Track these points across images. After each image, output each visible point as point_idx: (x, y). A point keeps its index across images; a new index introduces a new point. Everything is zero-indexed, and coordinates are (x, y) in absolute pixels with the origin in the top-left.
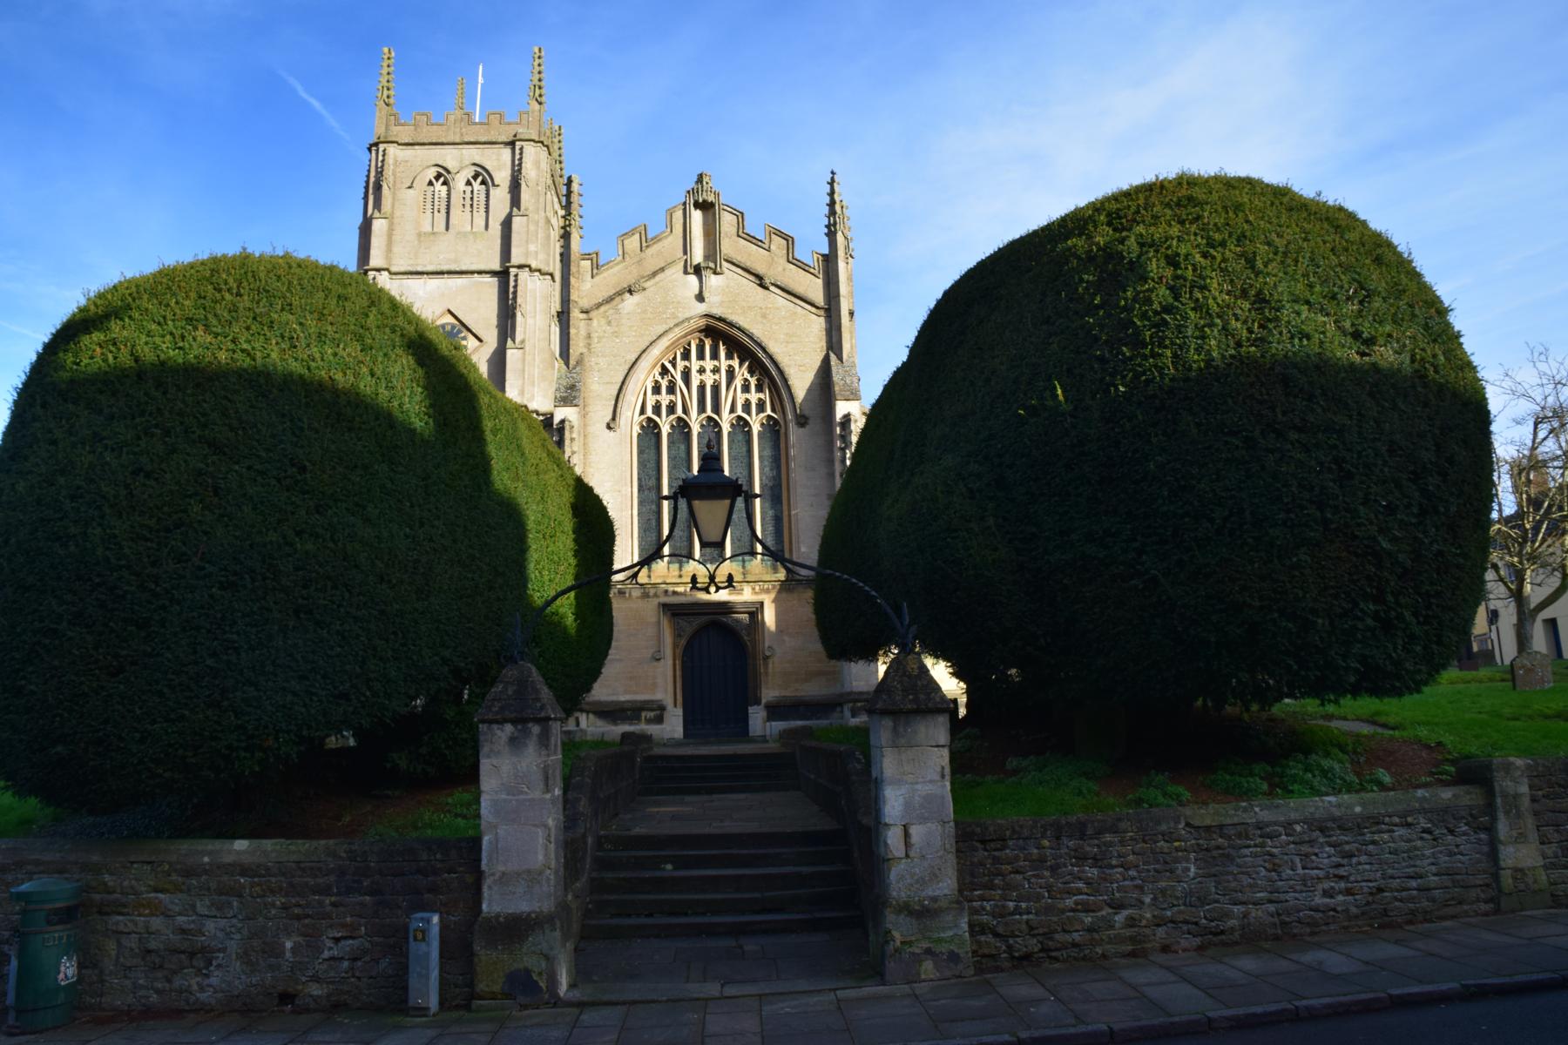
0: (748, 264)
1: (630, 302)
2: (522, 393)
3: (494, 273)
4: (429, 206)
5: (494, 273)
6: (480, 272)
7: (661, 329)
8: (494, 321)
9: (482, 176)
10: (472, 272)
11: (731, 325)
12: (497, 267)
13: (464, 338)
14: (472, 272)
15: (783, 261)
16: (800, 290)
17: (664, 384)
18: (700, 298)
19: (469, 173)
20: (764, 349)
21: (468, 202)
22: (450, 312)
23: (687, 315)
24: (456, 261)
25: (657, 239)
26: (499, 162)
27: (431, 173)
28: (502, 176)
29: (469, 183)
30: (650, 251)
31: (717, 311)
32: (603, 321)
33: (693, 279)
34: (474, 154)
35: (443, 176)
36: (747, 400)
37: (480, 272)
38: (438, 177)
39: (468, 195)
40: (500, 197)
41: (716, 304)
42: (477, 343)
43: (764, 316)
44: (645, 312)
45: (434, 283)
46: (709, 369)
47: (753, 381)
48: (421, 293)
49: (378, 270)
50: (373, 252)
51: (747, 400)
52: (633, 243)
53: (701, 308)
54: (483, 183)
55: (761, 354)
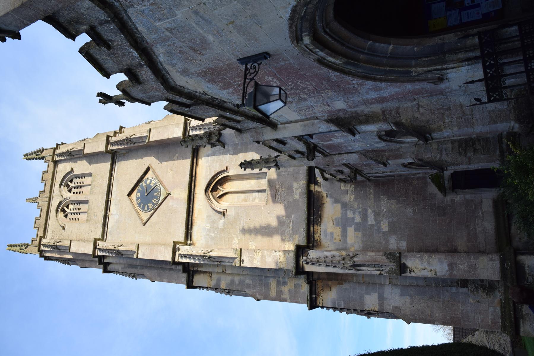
8: (139, 160)
21: (78, 190)
22: (129, 194)
29: (70, 191)
38: (64, 211)
49: (95, 248)
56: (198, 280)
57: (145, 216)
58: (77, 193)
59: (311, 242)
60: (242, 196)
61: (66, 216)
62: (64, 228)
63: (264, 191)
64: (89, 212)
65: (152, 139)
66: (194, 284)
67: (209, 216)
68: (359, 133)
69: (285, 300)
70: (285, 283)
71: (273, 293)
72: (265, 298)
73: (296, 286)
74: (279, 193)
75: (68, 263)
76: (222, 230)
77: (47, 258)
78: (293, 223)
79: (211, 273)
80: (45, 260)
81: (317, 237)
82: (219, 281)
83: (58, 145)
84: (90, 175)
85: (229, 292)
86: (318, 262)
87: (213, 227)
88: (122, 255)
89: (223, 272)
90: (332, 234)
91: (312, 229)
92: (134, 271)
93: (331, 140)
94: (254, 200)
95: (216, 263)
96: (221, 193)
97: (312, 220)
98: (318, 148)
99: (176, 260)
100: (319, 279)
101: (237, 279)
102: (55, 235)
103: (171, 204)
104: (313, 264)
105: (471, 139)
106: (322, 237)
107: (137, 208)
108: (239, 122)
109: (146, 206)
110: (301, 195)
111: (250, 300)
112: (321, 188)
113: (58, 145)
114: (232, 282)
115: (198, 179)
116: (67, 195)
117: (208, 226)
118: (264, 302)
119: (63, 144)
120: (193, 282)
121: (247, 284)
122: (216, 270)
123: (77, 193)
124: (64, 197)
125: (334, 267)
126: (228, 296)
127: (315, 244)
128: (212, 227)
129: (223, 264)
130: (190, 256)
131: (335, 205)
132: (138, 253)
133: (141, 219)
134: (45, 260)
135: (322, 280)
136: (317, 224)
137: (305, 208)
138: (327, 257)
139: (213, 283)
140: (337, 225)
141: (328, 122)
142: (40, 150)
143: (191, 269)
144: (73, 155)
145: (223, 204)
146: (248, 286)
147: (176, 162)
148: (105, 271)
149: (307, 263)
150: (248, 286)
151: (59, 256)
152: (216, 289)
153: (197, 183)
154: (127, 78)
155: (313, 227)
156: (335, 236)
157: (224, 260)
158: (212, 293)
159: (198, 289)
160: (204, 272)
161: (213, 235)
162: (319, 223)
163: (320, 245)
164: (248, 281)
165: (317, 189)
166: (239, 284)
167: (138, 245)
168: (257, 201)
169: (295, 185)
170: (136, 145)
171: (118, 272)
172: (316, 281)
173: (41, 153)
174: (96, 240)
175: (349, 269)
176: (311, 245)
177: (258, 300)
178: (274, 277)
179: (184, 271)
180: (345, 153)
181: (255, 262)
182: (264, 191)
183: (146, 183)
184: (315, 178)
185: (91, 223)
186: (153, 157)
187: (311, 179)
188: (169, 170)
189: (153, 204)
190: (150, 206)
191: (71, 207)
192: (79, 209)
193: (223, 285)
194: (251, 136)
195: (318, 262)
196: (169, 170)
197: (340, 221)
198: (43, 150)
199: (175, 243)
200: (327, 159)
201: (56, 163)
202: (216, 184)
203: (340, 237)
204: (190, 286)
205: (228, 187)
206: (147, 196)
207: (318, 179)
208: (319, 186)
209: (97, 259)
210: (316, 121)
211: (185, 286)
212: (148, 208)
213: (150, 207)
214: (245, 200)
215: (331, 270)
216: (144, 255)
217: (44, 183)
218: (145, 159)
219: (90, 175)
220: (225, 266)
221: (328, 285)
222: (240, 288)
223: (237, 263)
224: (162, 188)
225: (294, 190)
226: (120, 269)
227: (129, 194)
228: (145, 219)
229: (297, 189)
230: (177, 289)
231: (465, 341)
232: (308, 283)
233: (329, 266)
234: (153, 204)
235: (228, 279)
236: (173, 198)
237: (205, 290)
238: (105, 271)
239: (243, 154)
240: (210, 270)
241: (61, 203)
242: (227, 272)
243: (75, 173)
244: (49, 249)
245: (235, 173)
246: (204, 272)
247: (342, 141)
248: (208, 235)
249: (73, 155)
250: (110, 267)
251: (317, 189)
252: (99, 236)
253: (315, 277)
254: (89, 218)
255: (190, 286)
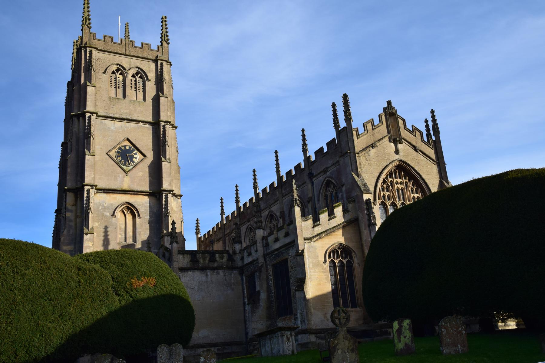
0: (409, 141)
1: (373, 151)
2: (170, 184)
3: (149, 123)
4: (113, 84)
5: (149, 123)
6: (143, 122)
7: (385, 164)
8: (151, 147)
9: (141, 74)
10: (139, 121)
11: (409, 165)
12: (150, 119)
13: (136, 154)
14: (139, 121)
15: (420, 141)
16: (427, 154)
17: (385, 186)
18: (397, 152)
19: (134, 71)
20: (421, 176)
21: (134, 86)
22: (128, 140)
23: (393, 159)
24: (130, 114)
25: (378, 126)
26: (150, 69)
27: (114, 68)
28: (152, 75)
29: (133, 76)
30: (376, 130)
31: (403, 159)
32: (364, 159)
33: (392, 144)
34: (136, 62)
35: (121, 70)
36: (384, 194)
37: (143, 122)
38: (118, 70)
39: (133, 82)
40: (151, 87)
41: (402, 156)
42: (143, 157)
43: (418, 163)
44: (378, 156)
45: (119, 124)
46: (399, 182)
47: (414, 188)
48: (112, 128)
49: (92, 113)
50: (88, 103)
51: (414, 196)
52: (369, 126)
53: (397, 157)
54: (140, 77)
55: (419, 178)
57: (113, 154)
60: (123, 227)
61: (113, 73)
63: (126, 241)
64: (117, 100)
65: (164, 164)
67: (112, 205)
76: (103, 215)
84: (144, 99)
87: (105, 208)
94: (121, 234)
96: (126, 212)
101: (73, 224)
102: (98, 63)
105: (103, 206)
107: (119, 146)
114: (71, 221)
115: (135, 196)
116: (131, 73)
117: (106, 205)
121: (69, 231)
124: (129, 71)
128: (105, 208)
130: (88, 197)
132: (89, 155)
133: (110, 151)
142: (168, 40)
144: (160, 81)
145: (119, 214)
146: (69, 231)
147: (148, 179)
151: (82, 68)
153: (132, 196)
157: (87, 221)
168: (120, 236)
173: (166, 42)
178: (75, 248)
181: (86, 242)
182: (126, 241)
185: (108, 102)
186: (152, 159)
188: (142, 173)
189: (121, 161)
190: (120, 158)
191: (121, 77)
192: (119, 88)
196: (142, 173)
198: (168, 44)
201: (156, 61)
202: (131, 209)
205: (129, 217)
206: (125, 156)
212: (118, 156)
214: (121, 229)
216: (88, 160)
217: (140, 46)
218: (152, 153)
219: (144, 99)
223: (86, 231)
224: (131, 167)
226: (75, 130)
227: (128, 140)
228: (111, 154)
231: (377, 229)
234: (121, 161)
235: (73, 218)
236: (124, 177)
239: (148, 227)
241: (124, 69)
243: (147, 83)
244: (88, 58)
245: (137, 223)
254: (112, 100)
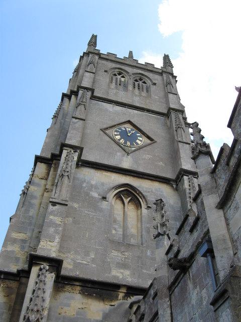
56: (42, 167)
58: (134, 85)
59: (63, 282)
62: (106, 71)
66: (38, 164)
67: (103, 184)
68: (215, 311)
69: (5, 245)
70: (22, 248)
71: (15, 235)
72: (10, 226)
73: (17, 259)
74: (120, 255)
75: (75, 72)
76: (87, 194)
77: (82, 58)
78: (86, 264)
79: (46, 179)
80: (81, 56)
81: (68, 288)
82: (38, 185)
83: (176, 77)
85: (24, 193)
86: (40, 281)
88: (77, 108)
89: (46, 189)
90: (69, 305)
91: (77, 284)
92: (60, 117)
93: (195, 287)
95: (56, 181)
97: (87, 285)
98: (183, 274)
99: (65, 148)
100: (21, 284)
103: (118, 154)
104: (39, 276)
106: (67, 294)
108: (228, 164)
109: (118, 133)
110: (115, 277)
111: (12, 212)
112: (122, 302)
113: (176, 77)
114: (33, 197)
117: (93, 183)
118: (8, 224)
119: (176, 81)
120: (41, 162)
121: (29, 211)
122: (49, 182)
123: (134, 85)
125: (31, 300)
126: (21, 192)
127: (60, 285)
128: (92, 186)
129: (55, 187)
131: (101, 315)
134: (81, 56)
135: (19, 289)
136: (81, 290)
137: (101, 279)
138: (44, 292)
139: (36, 180)
140: (78, 313)
141: (232, 267)
143: (54, 161)
148: (64, 95)
149: (41, 270)
150: (27, 211)
152: (30, 182)
154: (230, 147)
155: (80, 286)
156: (66, 308)
158: (27, 178)
159: (33, 167)
160: (48, 174)
161: (84, 185)
162: (82, 293)
163: (58, 291)
164: (32, 212)
165: (121, 295)
166: (30, 203)
167: (84, 120)
169: (127, 272)
170: (175, 132)
171: (61, 105)
172: (19, 281)
174: (92, 91)
175: (25, 316)
176: (60, 280)
177: (11, 219)
179: (53, 155)
180: (171, 313)
183: (139, 136)
184: (134, 295)
187: (132, 290)
189: (119, 140)
193: (32, 188)
194: (207, 184)
195: (40, 281)
197: (82, 317)
199: (81, 149)
200: (165, 291)
203: (63, 314)
204: (38, 159)
207: (132, 297)
208: (124, 298)
209: (76, 90)
210: (231, 253)
211: (39, 154)
213: (117, 137)
215: (28, 295)
220: (52, 190)
221: (11, 294)
222: (26, 203)
225: (122, 271)
229: (122, 273)
230: (37, 144)
232: (18, 271)
233: (33, 293)
237: (31, 173)
238: (64, 95)
240: (50, 178)
242: (45, 193)
246: (48, 174)
247: (194, 302)
248: (85, 181)
249: (167, 86)
250: (66, 100)
251: (121, 295)
252: (96, 94)
253: (24, 280)
255: (38, 159)
